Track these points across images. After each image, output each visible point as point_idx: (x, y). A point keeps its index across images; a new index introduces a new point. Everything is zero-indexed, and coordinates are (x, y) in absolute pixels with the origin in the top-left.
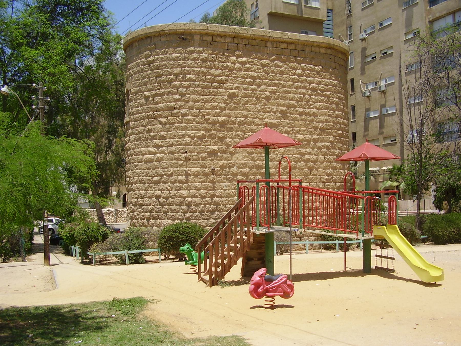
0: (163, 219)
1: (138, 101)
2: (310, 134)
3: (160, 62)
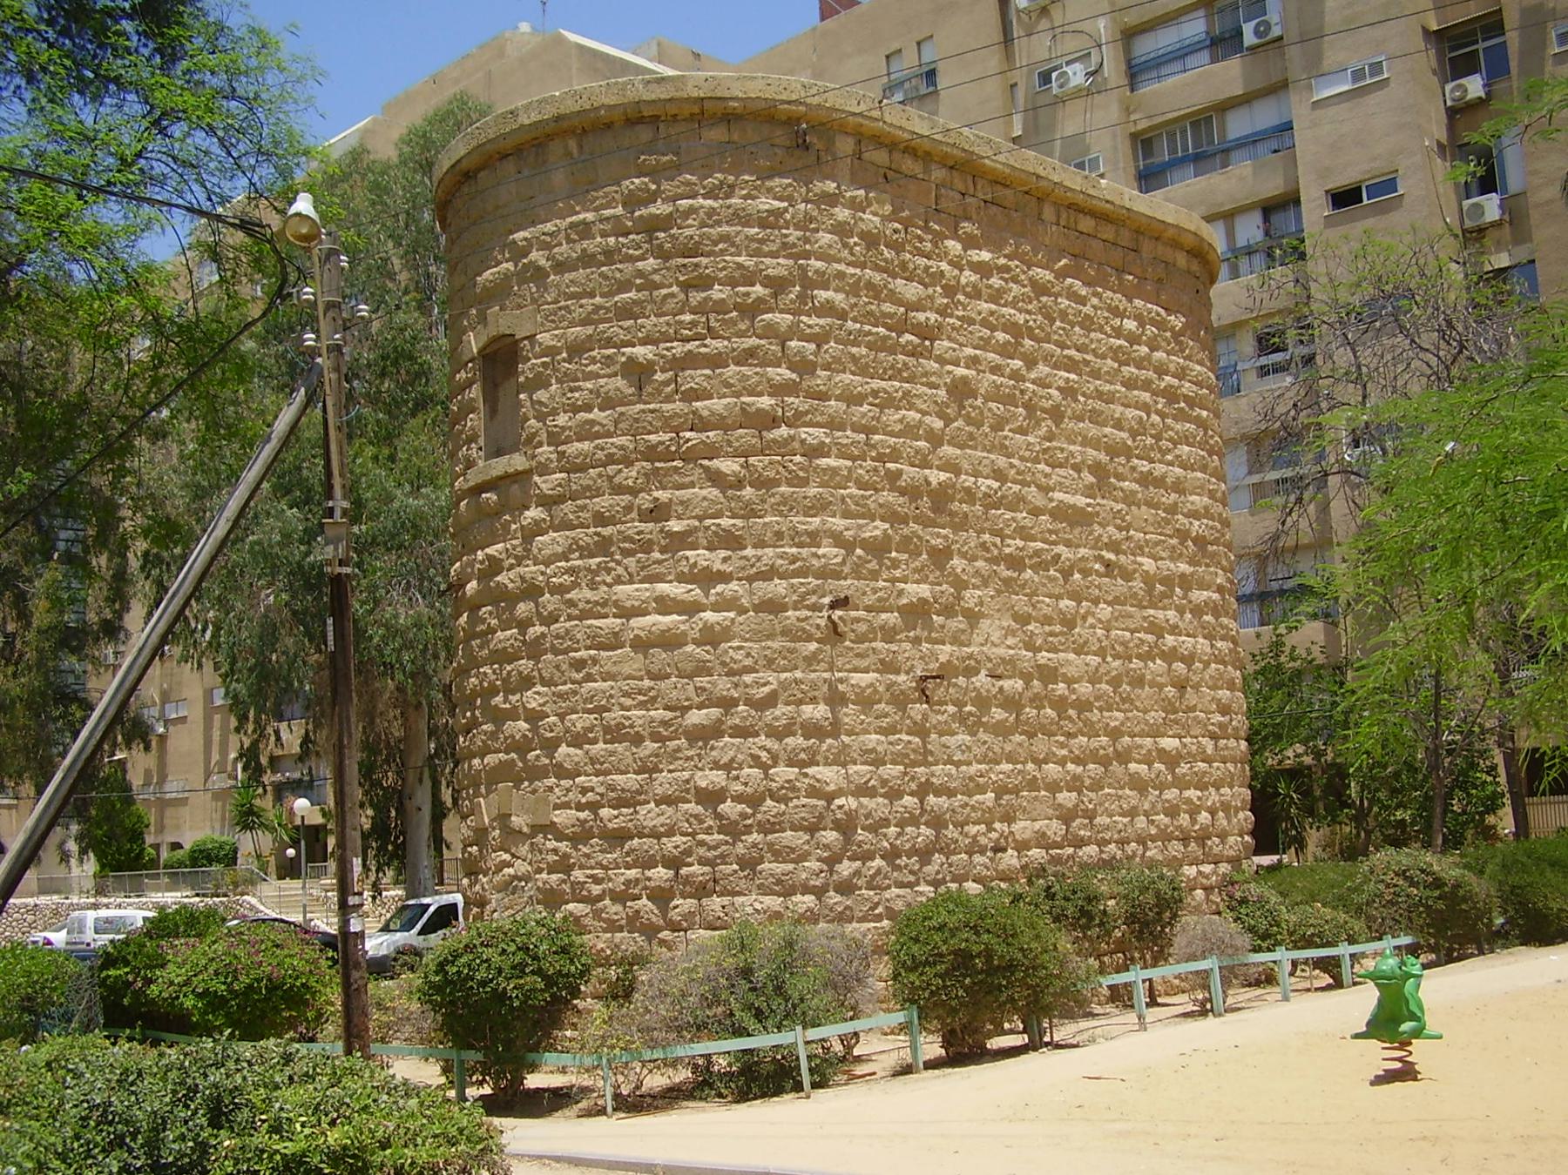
0: (739, 894)
1: (589, 385)
2: (1172, 559)
3: (703, 225)
